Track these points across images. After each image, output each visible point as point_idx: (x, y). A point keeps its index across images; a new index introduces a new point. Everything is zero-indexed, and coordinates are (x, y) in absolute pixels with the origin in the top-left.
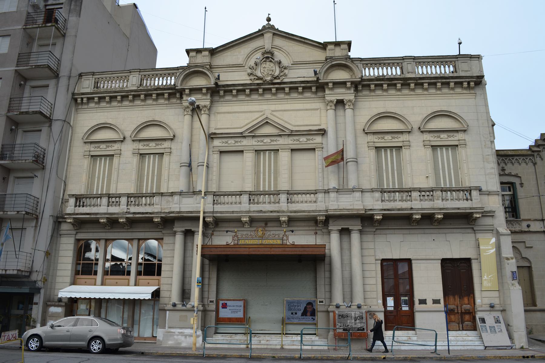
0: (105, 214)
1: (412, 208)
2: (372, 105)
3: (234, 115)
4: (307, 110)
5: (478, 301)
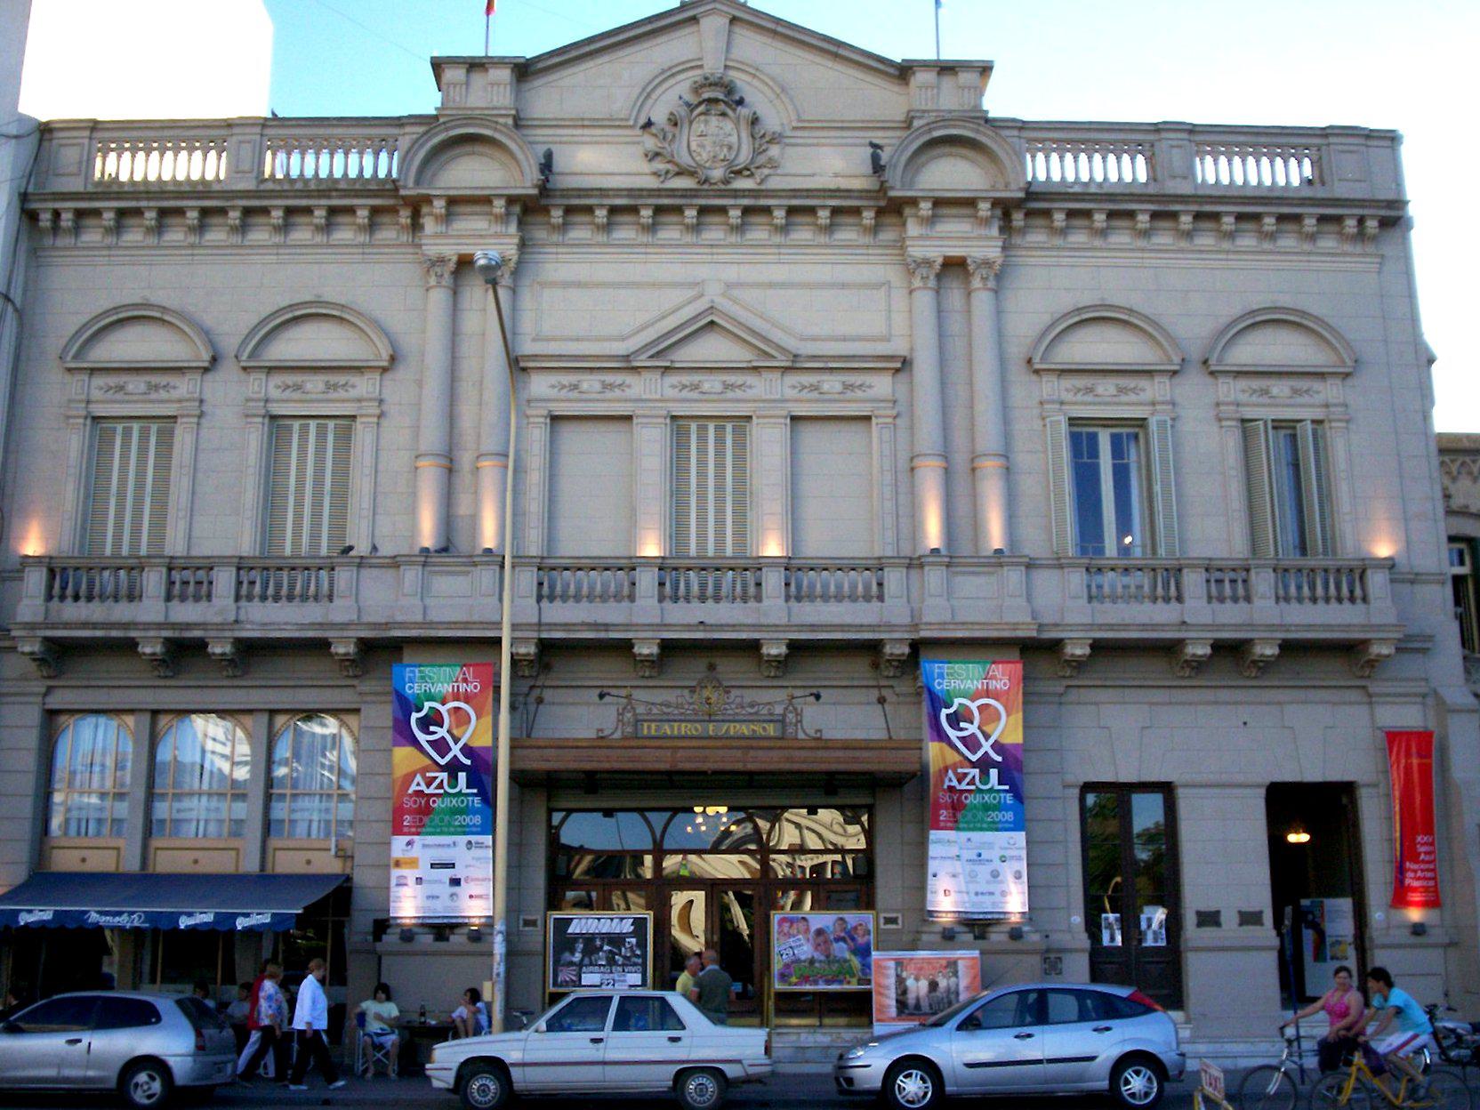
0: (160, 626)
2: (1056, 276)
3: (599, 294)
4: (844, 286)
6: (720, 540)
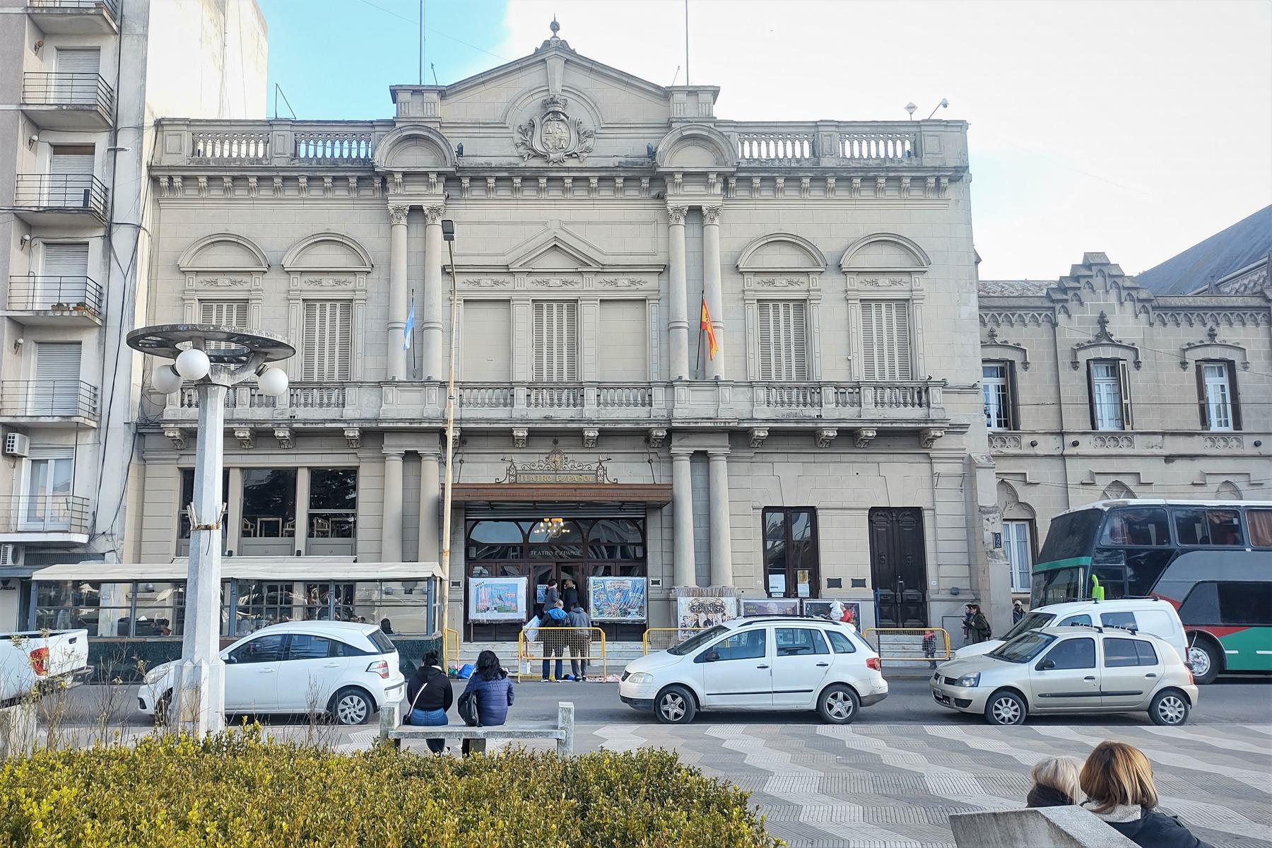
1: (752, 419)
3: (495, 227)
5: (932, 583)
6: (550, 373)
